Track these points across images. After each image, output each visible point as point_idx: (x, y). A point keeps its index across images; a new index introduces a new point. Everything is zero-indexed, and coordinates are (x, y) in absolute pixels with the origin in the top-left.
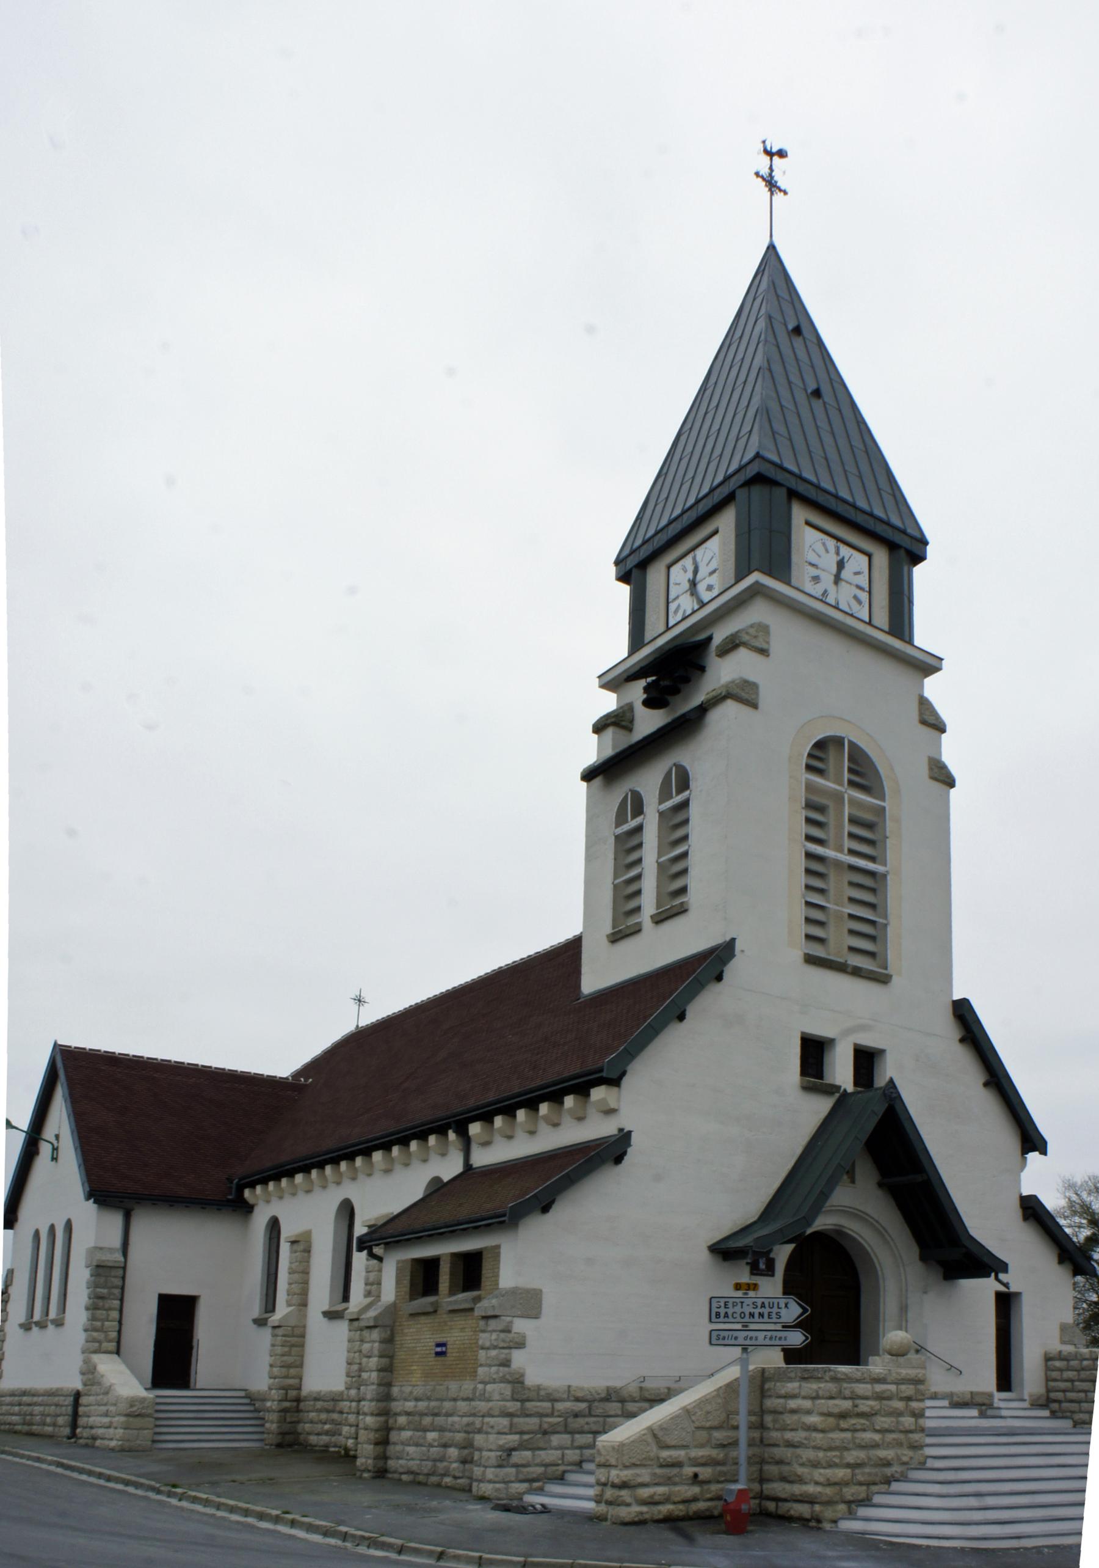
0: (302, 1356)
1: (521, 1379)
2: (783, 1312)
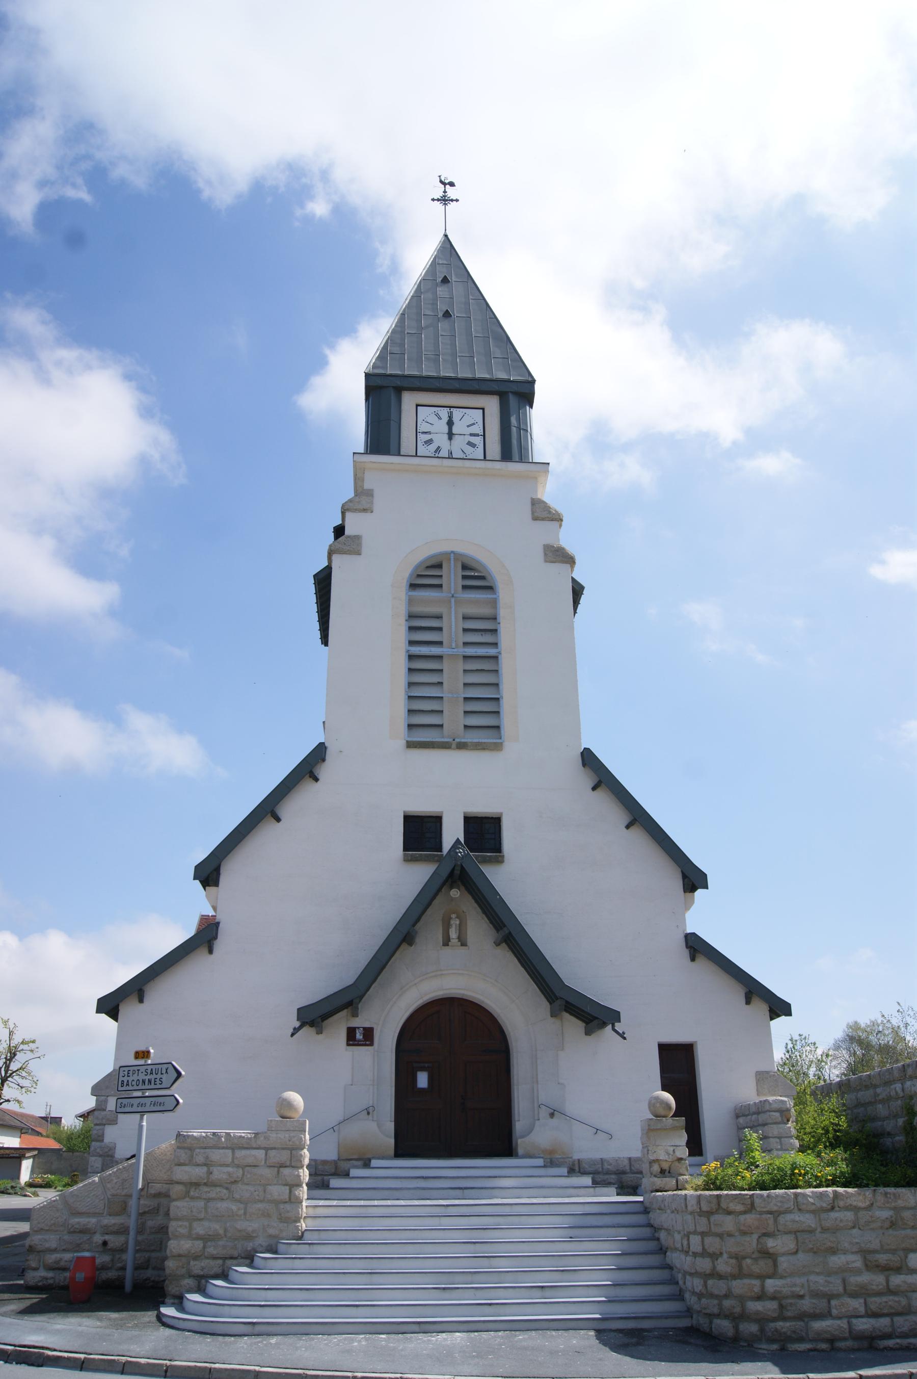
1: (110, 1153)
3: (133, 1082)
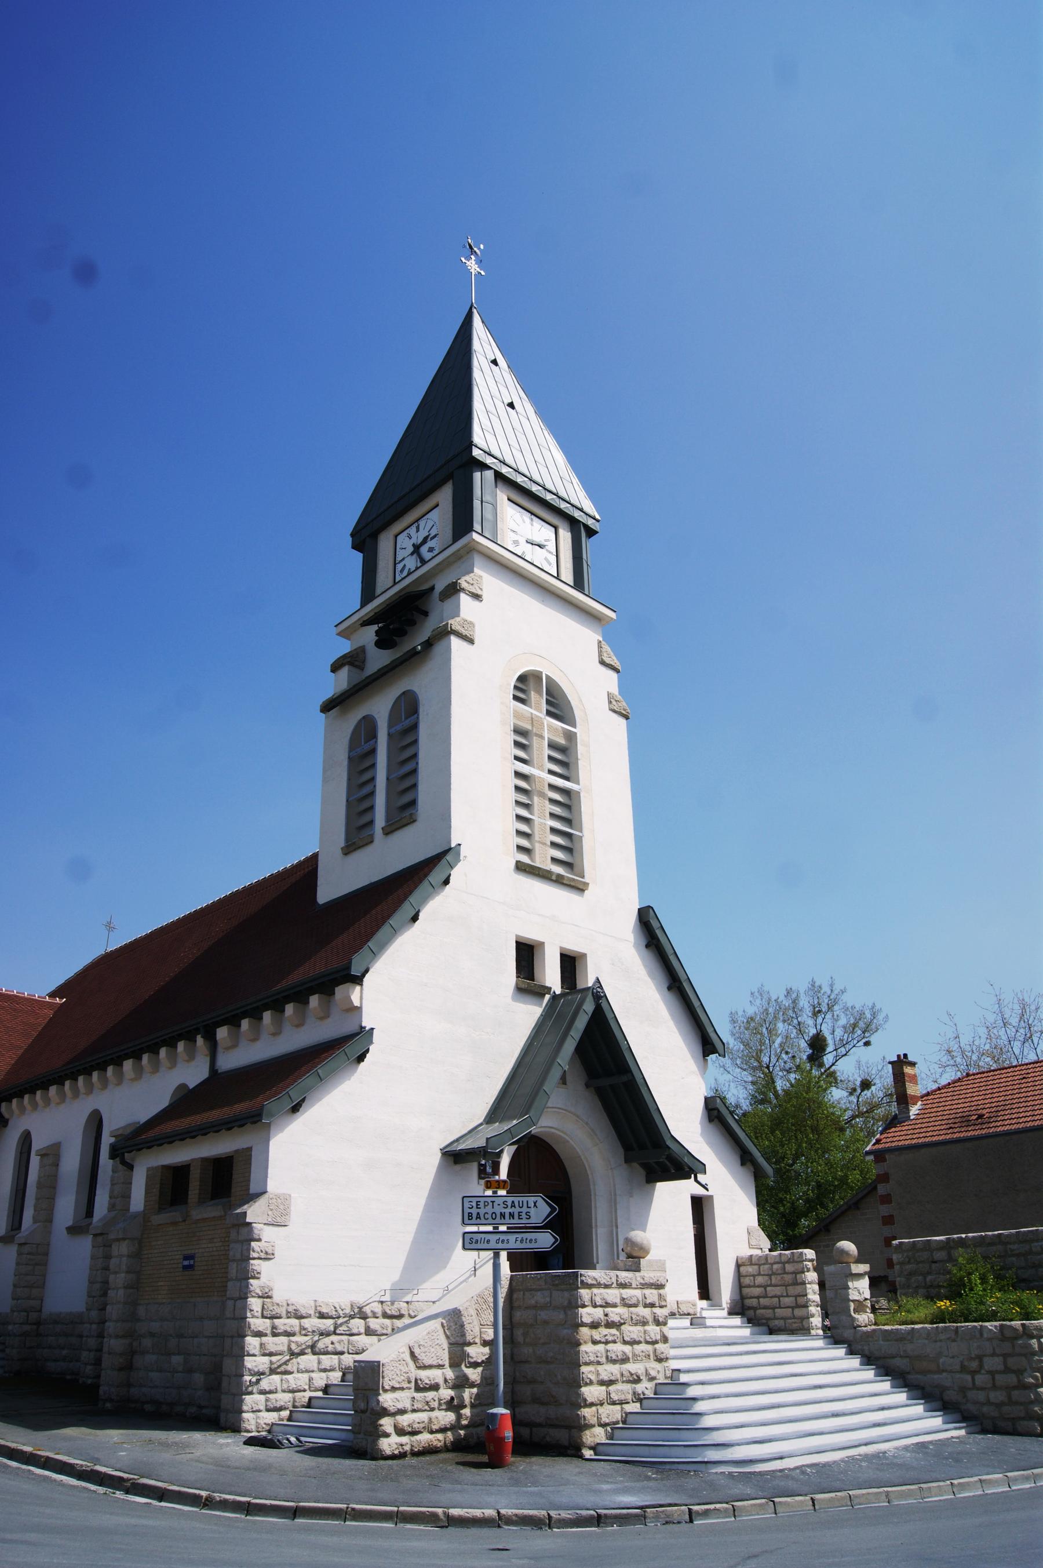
0: (44, 1276)
2: (533, 1211)
3: (486, 1215)
